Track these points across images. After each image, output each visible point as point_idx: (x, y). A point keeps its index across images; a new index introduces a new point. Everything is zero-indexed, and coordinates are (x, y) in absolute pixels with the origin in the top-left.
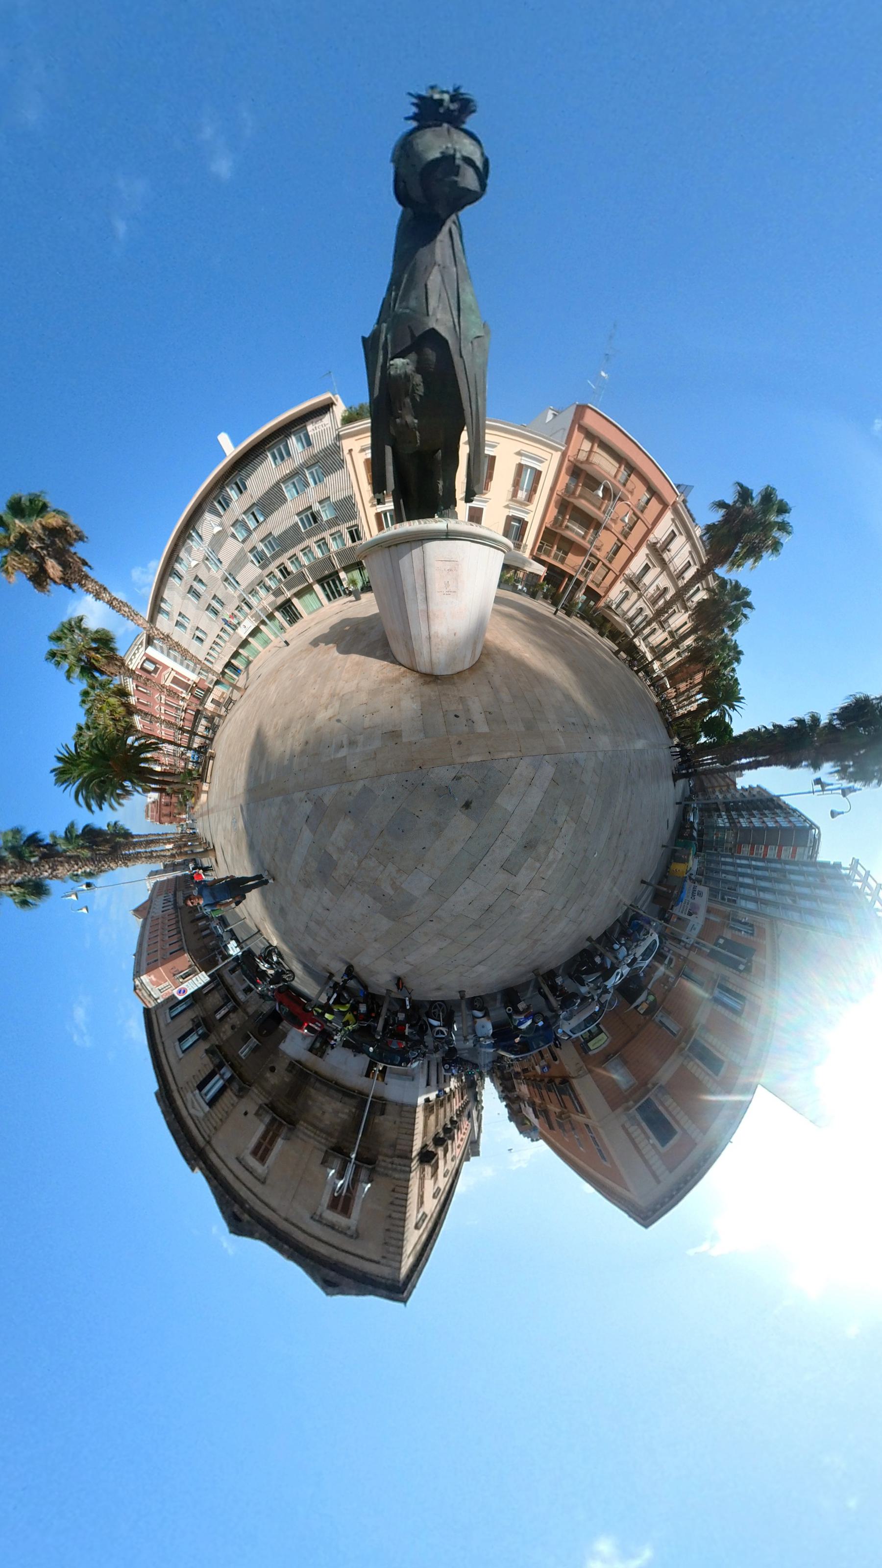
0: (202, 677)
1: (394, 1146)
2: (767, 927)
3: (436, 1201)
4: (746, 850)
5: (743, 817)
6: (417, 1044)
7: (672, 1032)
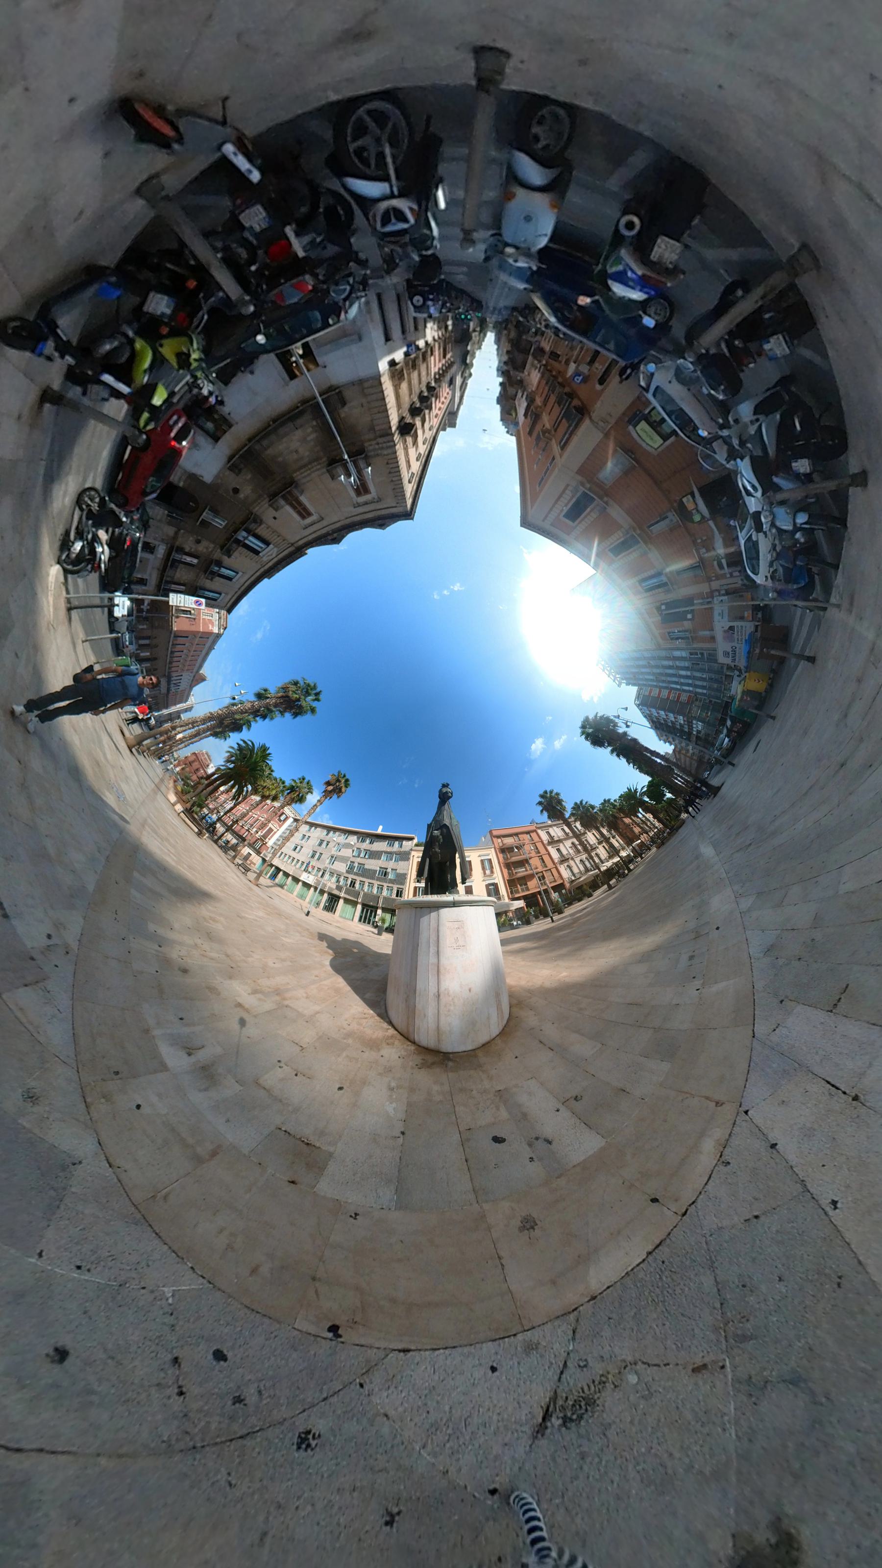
1: (372, 429)
2: (661, 641)
3: (419, 463)
4: (684, 697)
6: (339, 266)
7: (652, 525)
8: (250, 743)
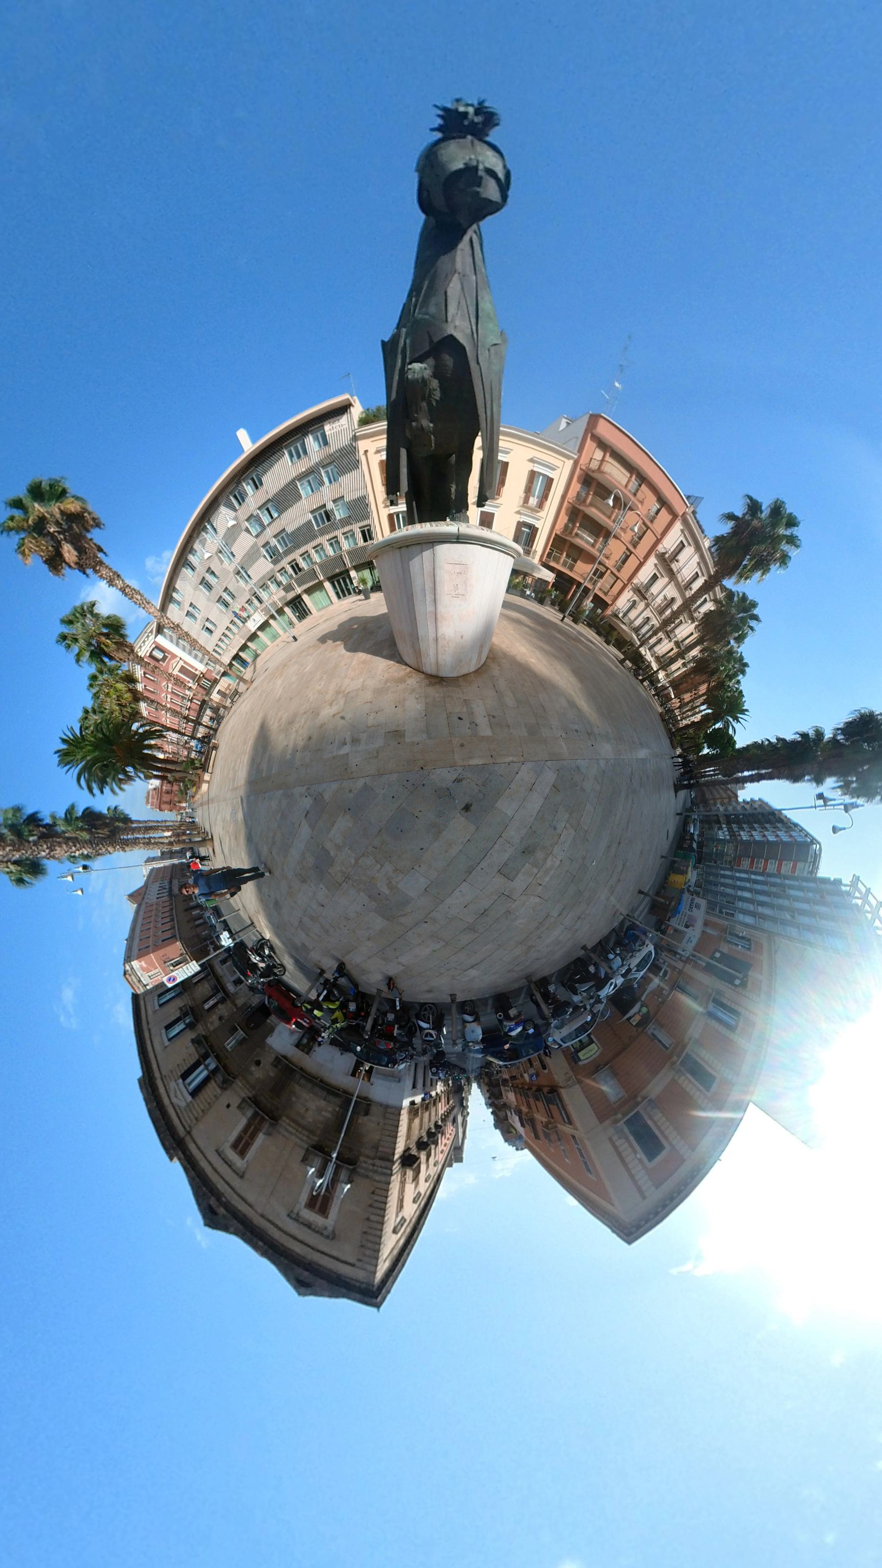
0: (210, 668)
1: (376, 1147)
3: (416, 1206)
4: (745, 864)
5: (744, 830)
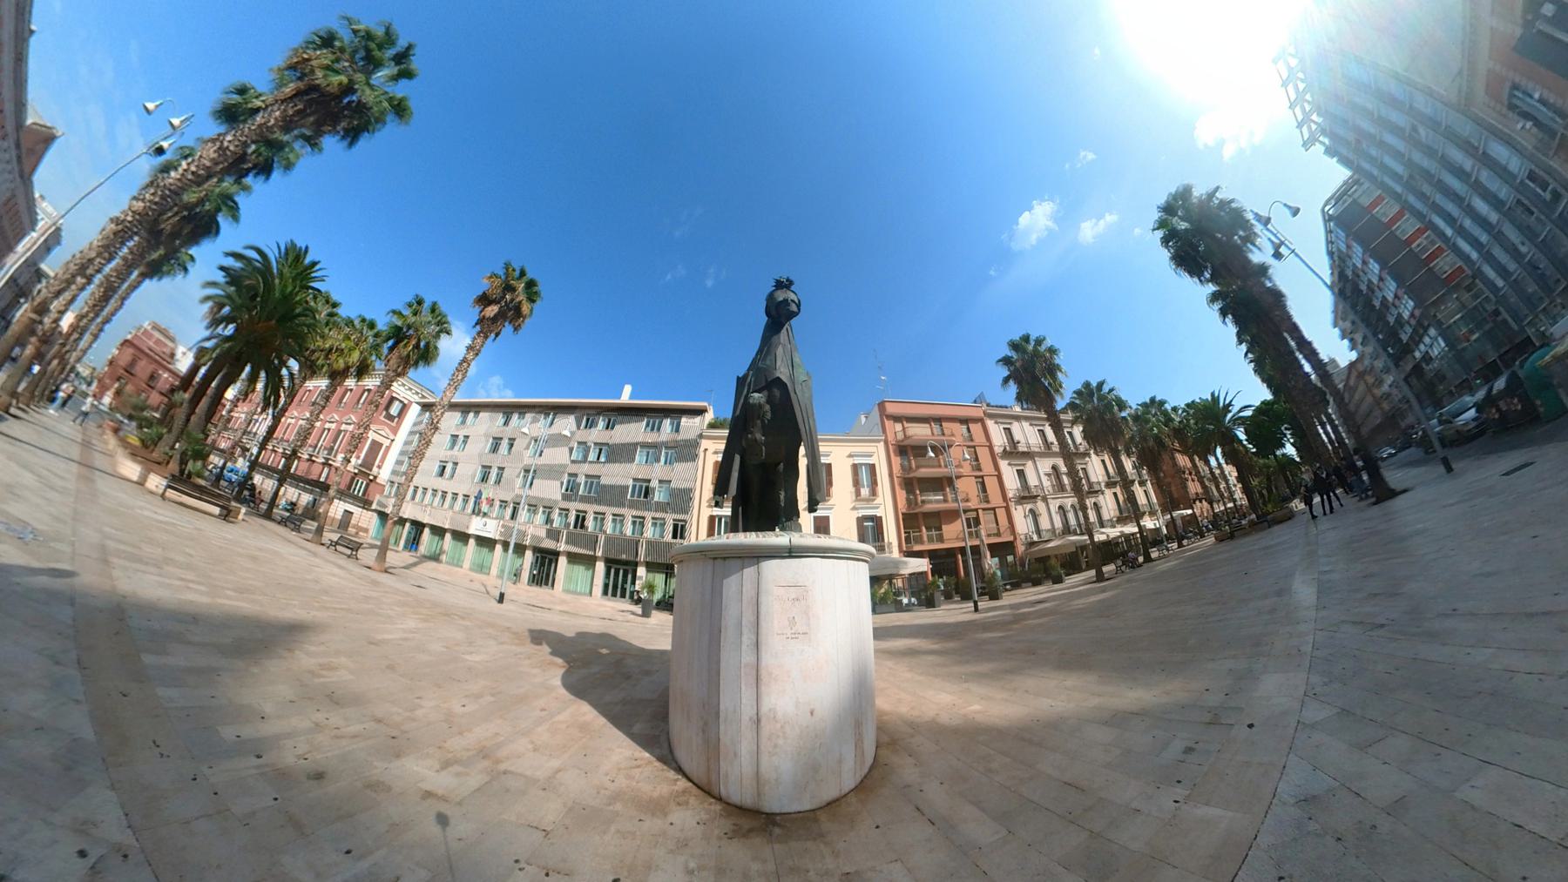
0: (387, 488)
4: (1445, 264)
5: (1400, 315)
8: (253, 254)
